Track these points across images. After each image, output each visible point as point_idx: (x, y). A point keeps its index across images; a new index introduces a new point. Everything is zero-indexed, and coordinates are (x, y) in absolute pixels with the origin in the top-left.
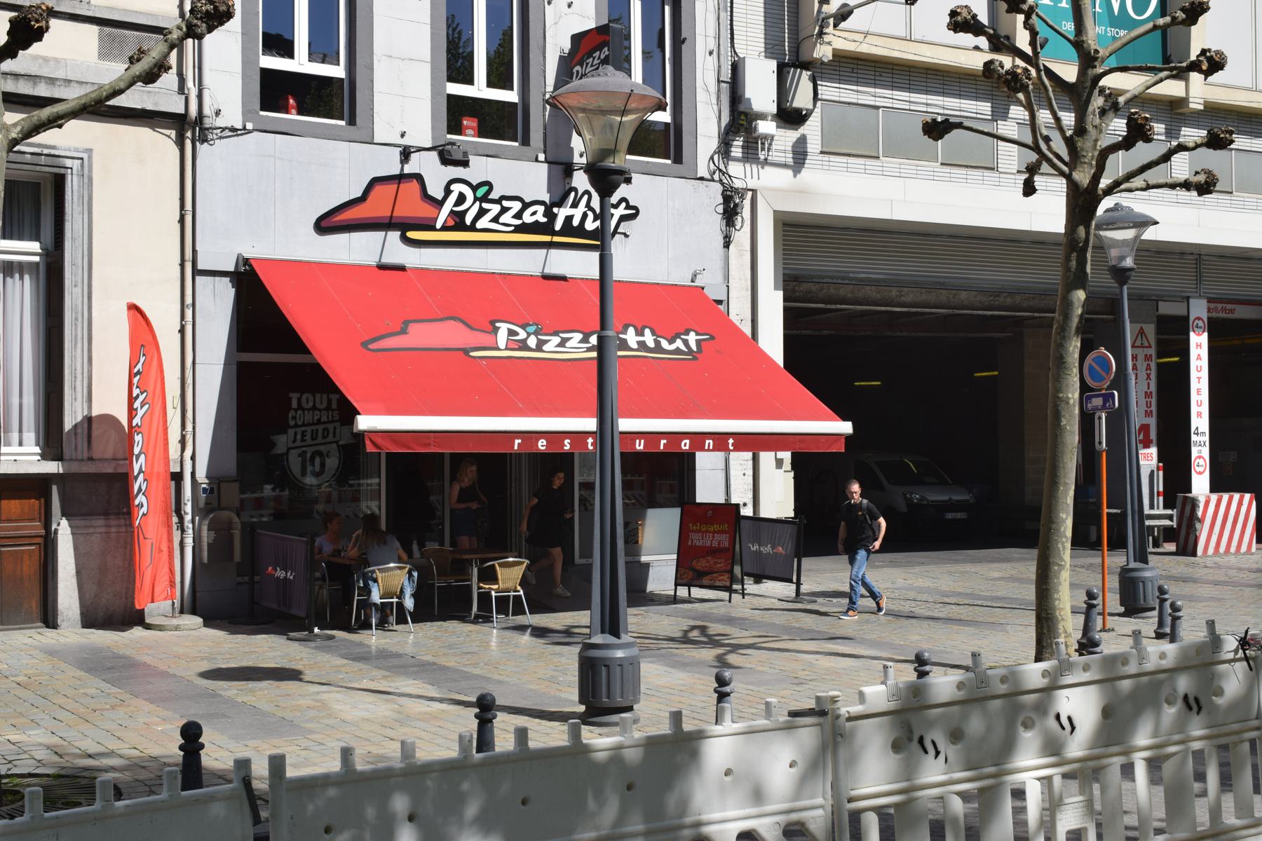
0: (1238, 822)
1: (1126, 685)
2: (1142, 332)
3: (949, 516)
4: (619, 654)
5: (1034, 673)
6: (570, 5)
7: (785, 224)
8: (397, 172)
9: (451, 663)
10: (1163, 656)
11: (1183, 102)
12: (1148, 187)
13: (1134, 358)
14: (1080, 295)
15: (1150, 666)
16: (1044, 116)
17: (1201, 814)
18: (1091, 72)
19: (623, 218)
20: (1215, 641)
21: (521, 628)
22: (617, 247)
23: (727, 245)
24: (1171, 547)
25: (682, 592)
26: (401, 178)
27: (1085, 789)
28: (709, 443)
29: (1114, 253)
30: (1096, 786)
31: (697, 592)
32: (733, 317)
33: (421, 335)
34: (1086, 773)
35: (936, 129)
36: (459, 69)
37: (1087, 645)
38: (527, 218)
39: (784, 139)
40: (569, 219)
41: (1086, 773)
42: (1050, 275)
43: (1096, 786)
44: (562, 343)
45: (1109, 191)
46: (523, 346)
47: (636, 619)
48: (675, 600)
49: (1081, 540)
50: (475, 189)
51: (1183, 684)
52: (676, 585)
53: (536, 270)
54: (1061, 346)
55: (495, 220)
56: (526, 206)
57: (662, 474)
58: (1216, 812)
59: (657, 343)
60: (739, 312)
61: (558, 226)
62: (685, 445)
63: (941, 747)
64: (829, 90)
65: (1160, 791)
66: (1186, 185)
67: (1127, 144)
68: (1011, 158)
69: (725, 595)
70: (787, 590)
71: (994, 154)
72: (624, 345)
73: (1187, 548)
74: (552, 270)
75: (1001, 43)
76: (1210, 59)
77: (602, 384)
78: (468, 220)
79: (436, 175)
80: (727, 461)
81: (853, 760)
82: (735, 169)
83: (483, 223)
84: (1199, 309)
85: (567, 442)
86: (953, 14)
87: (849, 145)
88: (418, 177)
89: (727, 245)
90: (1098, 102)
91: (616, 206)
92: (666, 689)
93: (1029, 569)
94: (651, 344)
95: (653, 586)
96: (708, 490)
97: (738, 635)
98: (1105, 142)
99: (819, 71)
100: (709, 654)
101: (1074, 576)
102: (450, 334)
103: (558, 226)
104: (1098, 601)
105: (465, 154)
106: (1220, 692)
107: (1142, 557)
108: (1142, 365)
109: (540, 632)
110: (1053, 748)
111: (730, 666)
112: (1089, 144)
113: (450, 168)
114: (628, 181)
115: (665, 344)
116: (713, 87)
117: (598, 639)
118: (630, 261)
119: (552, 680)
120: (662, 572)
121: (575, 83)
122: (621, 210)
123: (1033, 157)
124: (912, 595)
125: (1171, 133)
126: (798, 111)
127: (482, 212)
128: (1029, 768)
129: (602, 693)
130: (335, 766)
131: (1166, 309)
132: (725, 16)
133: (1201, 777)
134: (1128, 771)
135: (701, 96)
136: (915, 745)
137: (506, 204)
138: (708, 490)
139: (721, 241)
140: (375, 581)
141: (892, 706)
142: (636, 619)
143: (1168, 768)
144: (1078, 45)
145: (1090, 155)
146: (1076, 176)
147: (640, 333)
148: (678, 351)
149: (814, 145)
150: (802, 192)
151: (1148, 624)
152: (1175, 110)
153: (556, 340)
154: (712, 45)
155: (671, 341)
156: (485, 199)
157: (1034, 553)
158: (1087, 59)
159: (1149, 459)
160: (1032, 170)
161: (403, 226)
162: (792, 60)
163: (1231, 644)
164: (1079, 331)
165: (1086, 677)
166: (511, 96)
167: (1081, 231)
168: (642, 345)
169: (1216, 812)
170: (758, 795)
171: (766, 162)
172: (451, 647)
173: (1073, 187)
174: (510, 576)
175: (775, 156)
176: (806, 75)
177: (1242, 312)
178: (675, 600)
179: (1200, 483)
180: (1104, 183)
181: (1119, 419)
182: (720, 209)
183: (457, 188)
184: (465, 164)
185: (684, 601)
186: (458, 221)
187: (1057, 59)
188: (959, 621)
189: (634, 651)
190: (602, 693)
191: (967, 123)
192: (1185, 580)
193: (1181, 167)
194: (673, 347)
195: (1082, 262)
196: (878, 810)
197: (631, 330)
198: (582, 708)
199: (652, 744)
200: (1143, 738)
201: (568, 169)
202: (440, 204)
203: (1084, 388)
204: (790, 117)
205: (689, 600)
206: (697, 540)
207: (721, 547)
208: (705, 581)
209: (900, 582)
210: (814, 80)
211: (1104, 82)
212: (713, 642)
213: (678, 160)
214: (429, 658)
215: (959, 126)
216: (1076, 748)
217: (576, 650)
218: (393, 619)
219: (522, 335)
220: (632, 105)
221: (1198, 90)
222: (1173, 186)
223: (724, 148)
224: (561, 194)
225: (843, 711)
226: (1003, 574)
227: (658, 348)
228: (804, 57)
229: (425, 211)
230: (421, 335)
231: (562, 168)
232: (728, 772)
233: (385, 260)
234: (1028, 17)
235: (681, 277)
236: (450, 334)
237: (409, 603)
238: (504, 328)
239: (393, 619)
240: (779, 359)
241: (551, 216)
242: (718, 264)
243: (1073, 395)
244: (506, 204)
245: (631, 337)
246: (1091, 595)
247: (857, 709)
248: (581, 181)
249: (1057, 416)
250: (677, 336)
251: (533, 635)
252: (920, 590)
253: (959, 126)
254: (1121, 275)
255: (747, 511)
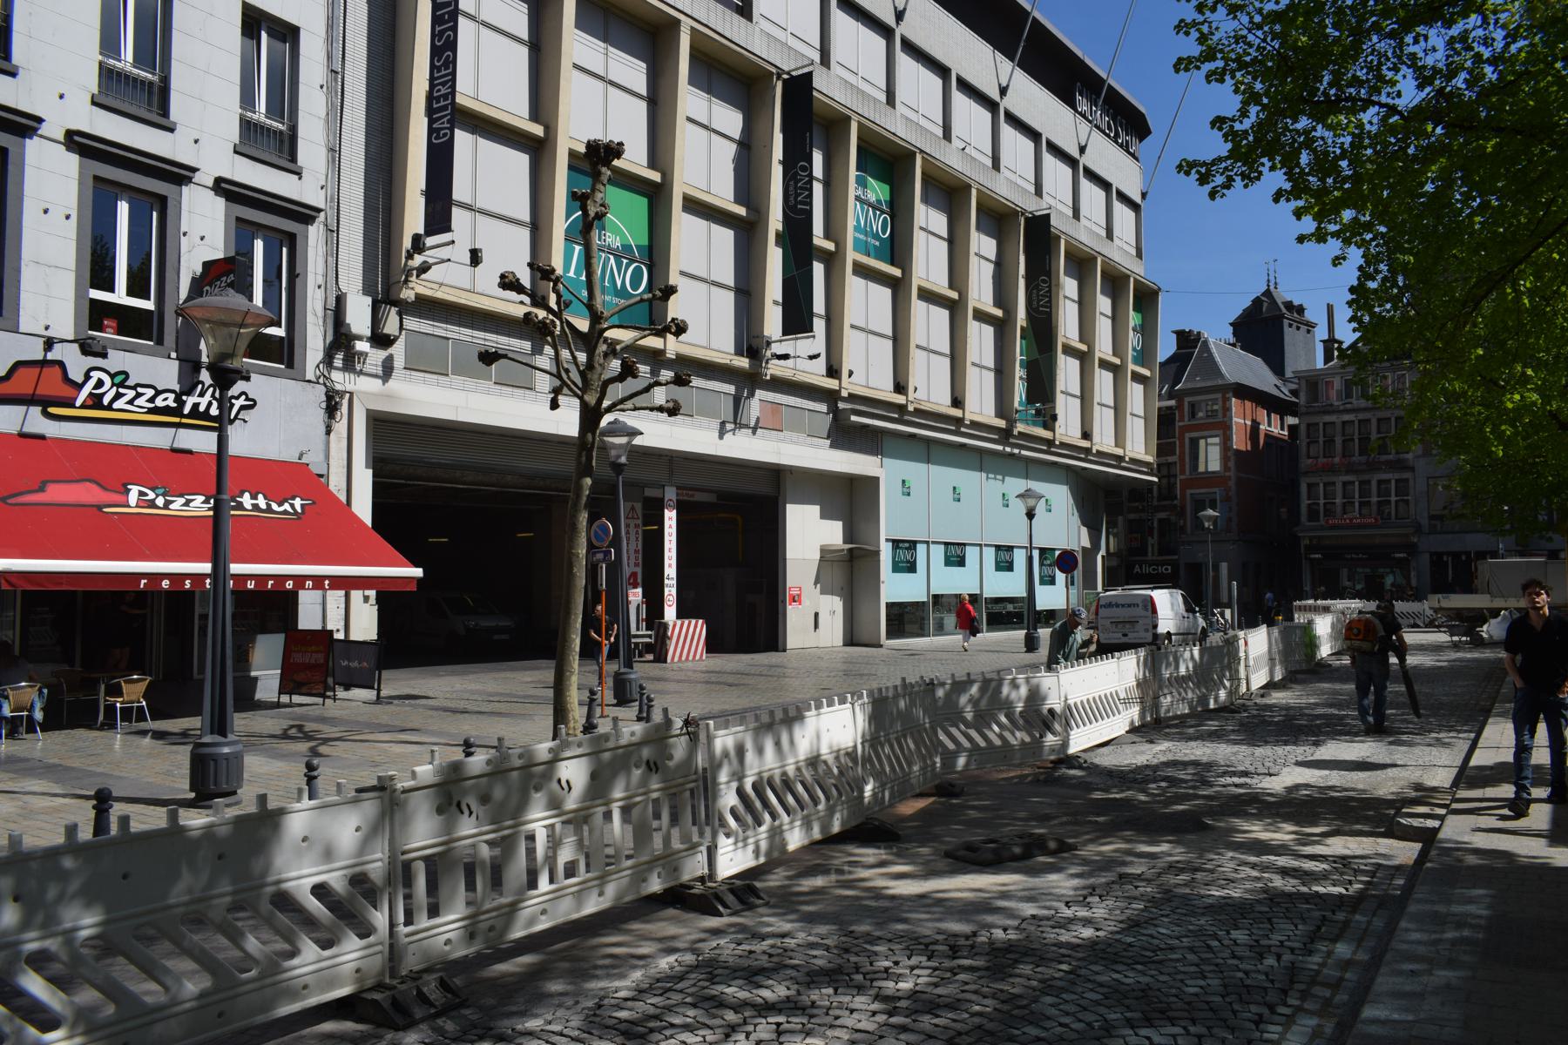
0: (682, 847)
1: (607, 756)
2: (633, 508)
3: (496, 637)
4: (226, 750)
5: (543, 749)
6: (202, 238)
7: (375, 420)
8: (40, 357)
9: (76, 763)
10: (633, 734)
11: (662, 352)
12: (635, 409)
13: (627, 526)
14: (588, 481)
15: (623, 742)
16: (565, 354)
17: (658, 841)
18: (598, 327)
19: (242, 408)
20: (668, 722)
21: (143, 733)
22: (235, 433)
23: (328, 432)
24: (650, 657)
25: (285, 699)
26: (44, 363)
27: (578, 832)
28: (309, 583)
29: (613, 453)
30: (586, 828)
31: (297, 699)
32: (332, 487)
33: (57, 493)
34: (578, 820)
35: (488, 358)
36: (101, 274)
37: (589, 727)
38: (159, 402)
39: (376, 356)
40: (196, 406)
41: (578, 820)
42: (568, 466)
43: (586, 828)
44: (187, 503)
45: (609, 410)
46: (152, 504)
47: (241, 722)
48: (278, 705)
49: (589, 651)
50: (113, 376)
51: (646, 752)
52: (280, 693)
53: (166, 445)
54: (574, 517)
55: (131, 402)
56: (158, 393)
57: (272, 607)
58: (667, 840)
59: (269, 506)
60: (336, 484)
61: (186, 411)
62: (289, 585)
63: (473, 808)
64: (412, 323)
65: (630, 828)
66: (660, 409)
67: (621, 378)
68: (544, 383)
69: (320, 700)
70: (369, 694)
71: (532, 379)
72: (240, 506)
73: (661, 658)
74: (178, 445)
75: (539, 301)
76: (677, 325)
77: (216, 537)
78: (106, 401)
79: (77, 364)
80: (324, 597)
81: (406, 822)
82: (337, 376)
83: (117, 405)
84: (671, 494)
85: (188, 582)
86: (503, 276)
87: (426, 362)
88: (61, 364)
89: (328, 432)
90: (603, 348)
91: (237, 398)
92: (264, 773)
93: (549, 675)
94: (263, 506)
95: (260, 695)
96: (308, 619)
97: (329, 731)
98: (606, 376)
99: (405, 308)
100: (303, 747)
101: (578, 676)
102: (86, 493)
103: (186, 411)
104: (598, 696)
105: (105, 348)
106: (671, 757)
107: (629, 665)
108: (632, 531)
109: (159, 735)
110: (555, 804)
111: (320, 755)
112: (596, 377)
113: (90, 358)
114: (248, 379)
115: (275, 506)
116: (320, 313)
117: (207, 739)
118: (242, 442)
119: (168, 773)
120: (268, 681)
121: (199, 301)
122: (238, 403)
123: (558, 383)
124: (466, 696)
125: (655, 373)
126: (388, 336)
127: (118, 396)
128: (538, 821)
129: (210, 779)
130: (60, 840)
131: (649, 492)
132: (331, 260)
133: (657, 816)
134: (608, 816)
135: (310, 318)
136: (454, 807)
137: (140, 390)
138: (308, 619)
139: (323, 429)
140: (7, 697)
141: (436, 780)
142: (241, 722)
143: (635, 812)
144: (590, 306)
145: (596, 384)
146: (586, 398)
147: (254, 497)
148: (285, 512)
149: (399, 362)
150: (389, 397)
151: (631, 712)
152: (656, 358)
153: (182, 501)
154: (320, 280)
155: (280, 505)
156: (122, 385)
157: (552, 663)
158: (596, 318)
159: (636, 596)
160: (556, 391)
161: (45, 403)
162: (384, 296)
163: (678, 723)
164: (586, 506)
165: (579, 751)
166: (149, 305)
167: (589, 436)
168: (256, 507)
169: (667, 840)
170: (328, 854)
171: (361, 373)
172: (76, 751)
173: (584, 407)
174: (134, 691)
175: (368, 368)
176: (394, 310)
177: (699, 497)
178: (278, 705)
179: (670, 613)
180: (606, 403)
181: (615, 568)
182: (324, 405)
183: (96, 375)
184: (104, 356)
185: (286, 706)
186: (96, 401)
187: (577, 315)
188: (500, 714)
189: (239, 747)
190: (210, 779)
191: (511, 355)
192: (658, 680)
193: (660, 396)
194: (281, 509)
195: (590, 458)
196: (426, 859)
197: (247, 495)
198: (193, 795)
199: (240, 821)
200: (618, 793)
201: (197, 367)
202: (80, 387)
203: (591, 547)
204: (381, 340)
205: (290, 705)
206: (298, 658)
207: (318, 663)
208: (304, 690)
209: (458, 686)
210: (400, 314)
211: (607, 334)
212: (308, 737)
213: (290, 365)
214: (55, 761)
215: (505, 356)
216: (571, 803)
217: (189, 748)
218: (23, 729)
219: (151, 495)
220: (249, 320)
221: (672, 346)
222: (652, 409)
223: (328, 360)
224: (189, 385)
225: (399, 786)
226: (532, 679)
227: (269, 509)
228: (393, 297)
229: (67, 391)
230: (57, 493)
231: (190, 367)
232: (305, 839)
233: (26, 429)
234: (555, 285)
235: (290, 455)
236: (86, 493)
237: (39, 715)
238: (134, 490)
239: (23, 729)
240: (369, 522)
241: (181, 404)
242: (321, 446)
243: (582, 551)
244: (140, 390)
245: (246, 500)
246: (592, 693)
247: (410, 784)
248: (205, 376)
249: (571, 566)
250: (286, 500)
251: (153, 737)
252: (473, 692)
253: (505, 356)
254: (618, 468)
255: (340, 636)
